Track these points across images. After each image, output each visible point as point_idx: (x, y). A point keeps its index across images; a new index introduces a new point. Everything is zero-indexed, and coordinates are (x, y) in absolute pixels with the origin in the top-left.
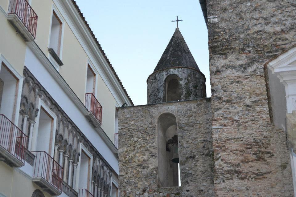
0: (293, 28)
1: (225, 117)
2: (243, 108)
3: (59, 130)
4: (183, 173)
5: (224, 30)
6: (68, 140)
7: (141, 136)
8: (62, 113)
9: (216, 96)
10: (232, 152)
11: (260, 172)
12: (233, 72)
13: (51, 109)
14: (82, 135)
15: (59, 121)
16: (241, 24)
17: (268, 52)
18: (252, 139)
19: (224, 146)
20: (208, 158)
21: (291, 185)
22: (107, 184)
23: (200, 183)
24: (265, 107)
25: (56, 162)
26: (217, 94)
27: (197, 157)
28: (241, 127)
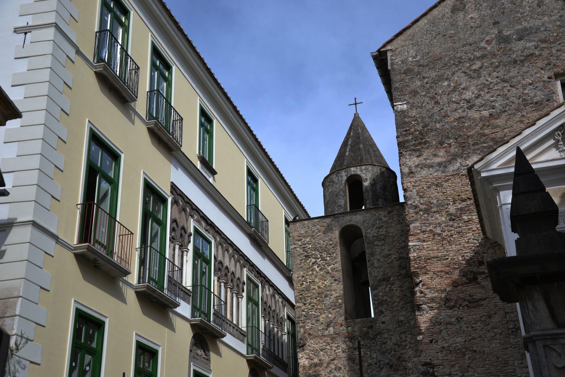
0: (505, 111)
1: (424, 230)
2: (446, 218)
3: (217, 255)
4: (376, 300)
5: (416, 119)
6: (229, 267)
7: (319, 256)
8: (220, 234)
9: (411, 204)
10: (435, 274)
11: (473, 299)
12: (431, 172)
13: (206, 230)
14: (246, 258)
15: (216, 244)
16: (436, 109)
17: (473, 145)
18: (460, 256)
19: (425, 267)
20: (406, 280)
21: (515, 313)
22: (281, 316)
23: (398, 312)
24: (474, 215)
25: (217, 296)
26: (412, 202)
27: (392, 279)
28: (445, 242)
